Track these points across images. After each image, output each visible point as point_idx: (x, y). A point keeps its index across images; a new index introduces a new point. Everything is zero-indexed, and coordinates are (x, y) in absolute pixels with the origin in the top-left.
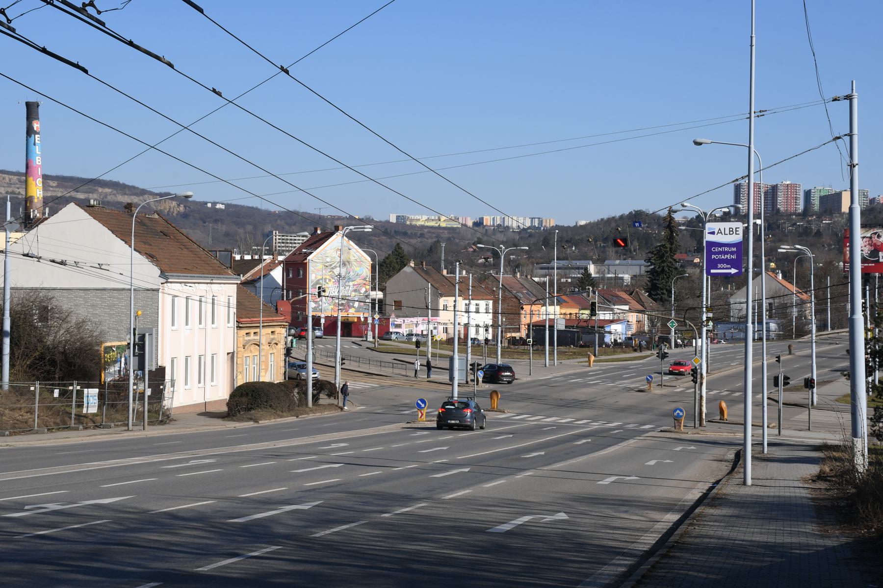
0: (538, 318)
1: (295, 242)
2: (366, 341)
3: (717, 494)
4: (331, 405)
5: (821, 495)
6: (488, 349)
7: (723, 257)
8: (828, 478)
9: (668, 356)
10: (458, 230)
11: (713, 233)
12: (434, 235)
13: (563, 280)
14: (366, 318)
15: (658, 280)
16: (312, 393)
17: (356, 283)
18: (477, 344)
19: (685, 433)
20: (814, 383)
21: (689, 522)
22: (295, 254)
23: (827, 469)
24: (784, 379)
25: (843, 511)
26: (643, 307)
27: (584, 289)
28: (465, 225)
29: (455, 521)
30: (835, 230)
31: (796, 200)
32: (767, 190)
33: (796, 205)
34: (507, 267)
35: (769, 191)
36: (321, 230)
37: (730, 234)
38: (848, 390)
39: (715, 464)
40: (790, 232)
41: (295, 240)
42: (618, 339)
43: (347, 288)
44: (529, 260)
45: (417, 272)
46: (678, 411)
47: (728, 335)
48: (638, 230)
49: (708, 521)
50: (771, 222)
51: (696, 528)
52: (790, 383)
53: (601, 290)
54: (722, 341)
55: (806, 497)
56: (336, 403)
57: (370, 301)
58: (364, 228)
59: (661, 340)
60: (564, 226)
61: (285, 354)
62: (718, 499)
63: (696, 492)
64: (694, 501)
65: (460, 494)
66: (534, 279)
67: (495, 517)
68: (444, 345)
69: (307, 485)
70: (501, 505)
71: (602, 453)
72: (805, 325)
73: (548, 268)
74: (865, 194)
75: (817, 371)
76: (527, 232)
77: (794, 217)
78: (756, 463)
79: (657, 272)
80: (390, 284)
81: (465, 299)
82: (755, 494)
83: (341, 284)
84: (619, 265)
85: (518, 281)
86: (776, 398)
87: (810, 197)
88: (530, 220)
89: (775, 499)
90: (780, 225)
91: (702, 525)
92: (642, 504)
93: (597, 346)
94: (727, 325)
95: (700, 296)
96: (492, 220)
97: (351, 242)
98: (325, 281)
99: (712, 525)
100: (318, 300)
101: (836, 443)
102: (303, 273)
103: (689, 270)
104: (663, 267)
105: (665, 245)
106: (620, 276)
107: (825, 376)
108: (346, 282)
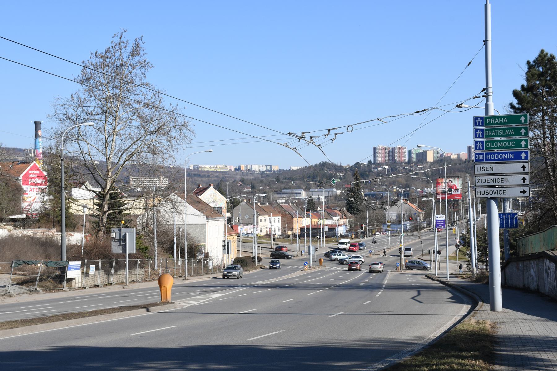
10: (227, 173)
28: (230, 170)
84: (317, 191)
87: (411, 154)
88: (265, 167)
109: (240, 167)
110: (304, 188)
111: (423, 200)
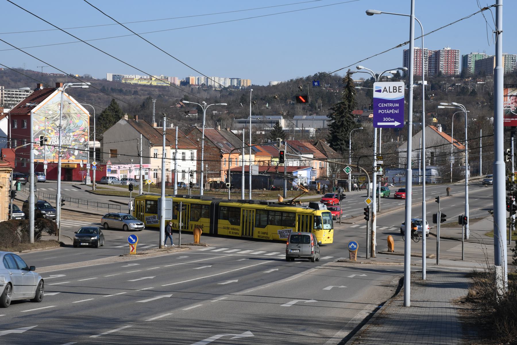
0: (236, 165)
1: (21, 96)
2: (85, 184)
3: (381, 314)
4: (52, 241)
5: (467, 314)
6: (193, 192)
7: (388, 112)
8: (475, 300)
9: (345, 198)
10: (167, 89)
11: (379, 91)
12: (146, 93)
13: (258, 133)
14: (85, 165)
15: (338, 132)
16: (35, 231)
17: (76, 134)
18: (184, 187)
19: (358, 263)
20: (467, 220)
21: (355, 338)
22: (20, 107)
23: (474, 293)
24: (441, 216)
25: (485, 328)
26: (325, 155)
27: (275, 140)
28: (173, 85)
29: (155, 341)
30: (487, 89)
31: (455, 64)
32: (431, 55)
33: (455, 68)
34: (210, 121)
35: (432, 56)
36: (43, 86)
37: (394, 92)
38: (491, 227)
39: (382, 289)
40: (450, 91)
41: (20, 95)
42: (304, 183)
43: (68, 138)
44: (229, 115)
45: (131, 125)
46: (352, 244)
47: (396, 180)
48: (322, 89)
49: (371, 337)
50: (434, 83)
51: (361, 343)
52: (447, 220)
53: (290, 141)
54: (391, 184)
55: (455, 316)
56: (57, 240)
57: (89, 150)
58: (82, 85)
59: (340, 183)
60: (259, 86)
61: (9, 196)
62: (381, 318)
63: (364, 313)
64: (362, 320)
65: (161, 317)
66: (232, 131)
67: (190, 336)
68: (154, 189)
69: (24, 311)
70: (196, 325)
71: (287, 281)
72: (461, 171)
73: (245, 122)
74: (514, 58)
75: (469, 210)
76: (227, 91)
77: (453, 78)
78: (416, 288)
79: (337, 126)
80: (106, 135)
81: (173, 148)
82: (413, 313)
83: (61, 135)
84: (306, 119)
85: (219, 133)
86: (435, 233)
87: (467, 61)
89: (429, 318)
90: (441, 85)
91: (366, 340)
92: (318, 323)
93: (286, 189)
94: (395, 171)
95: (372, 146)
96: (197, 80)
97: (71, 97)
98: (48, 132)
99: (374, 341)
100: (42, 148)
101: (482, 270)
102: (27, 125)
103: (365, 124)
104: (343, 121)
105: (344, 102)
106: (306, 129)
107: (476, 214)
108: (67, 133)
109: (188, 79)
110: (285, 114)
111: (439, 107)
